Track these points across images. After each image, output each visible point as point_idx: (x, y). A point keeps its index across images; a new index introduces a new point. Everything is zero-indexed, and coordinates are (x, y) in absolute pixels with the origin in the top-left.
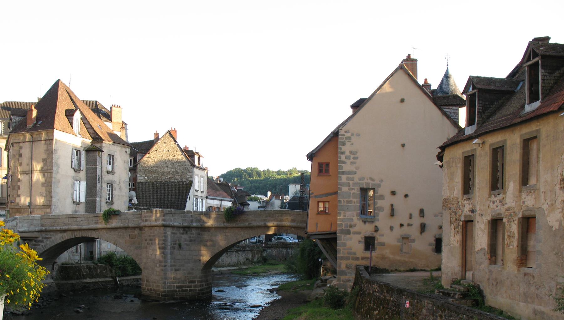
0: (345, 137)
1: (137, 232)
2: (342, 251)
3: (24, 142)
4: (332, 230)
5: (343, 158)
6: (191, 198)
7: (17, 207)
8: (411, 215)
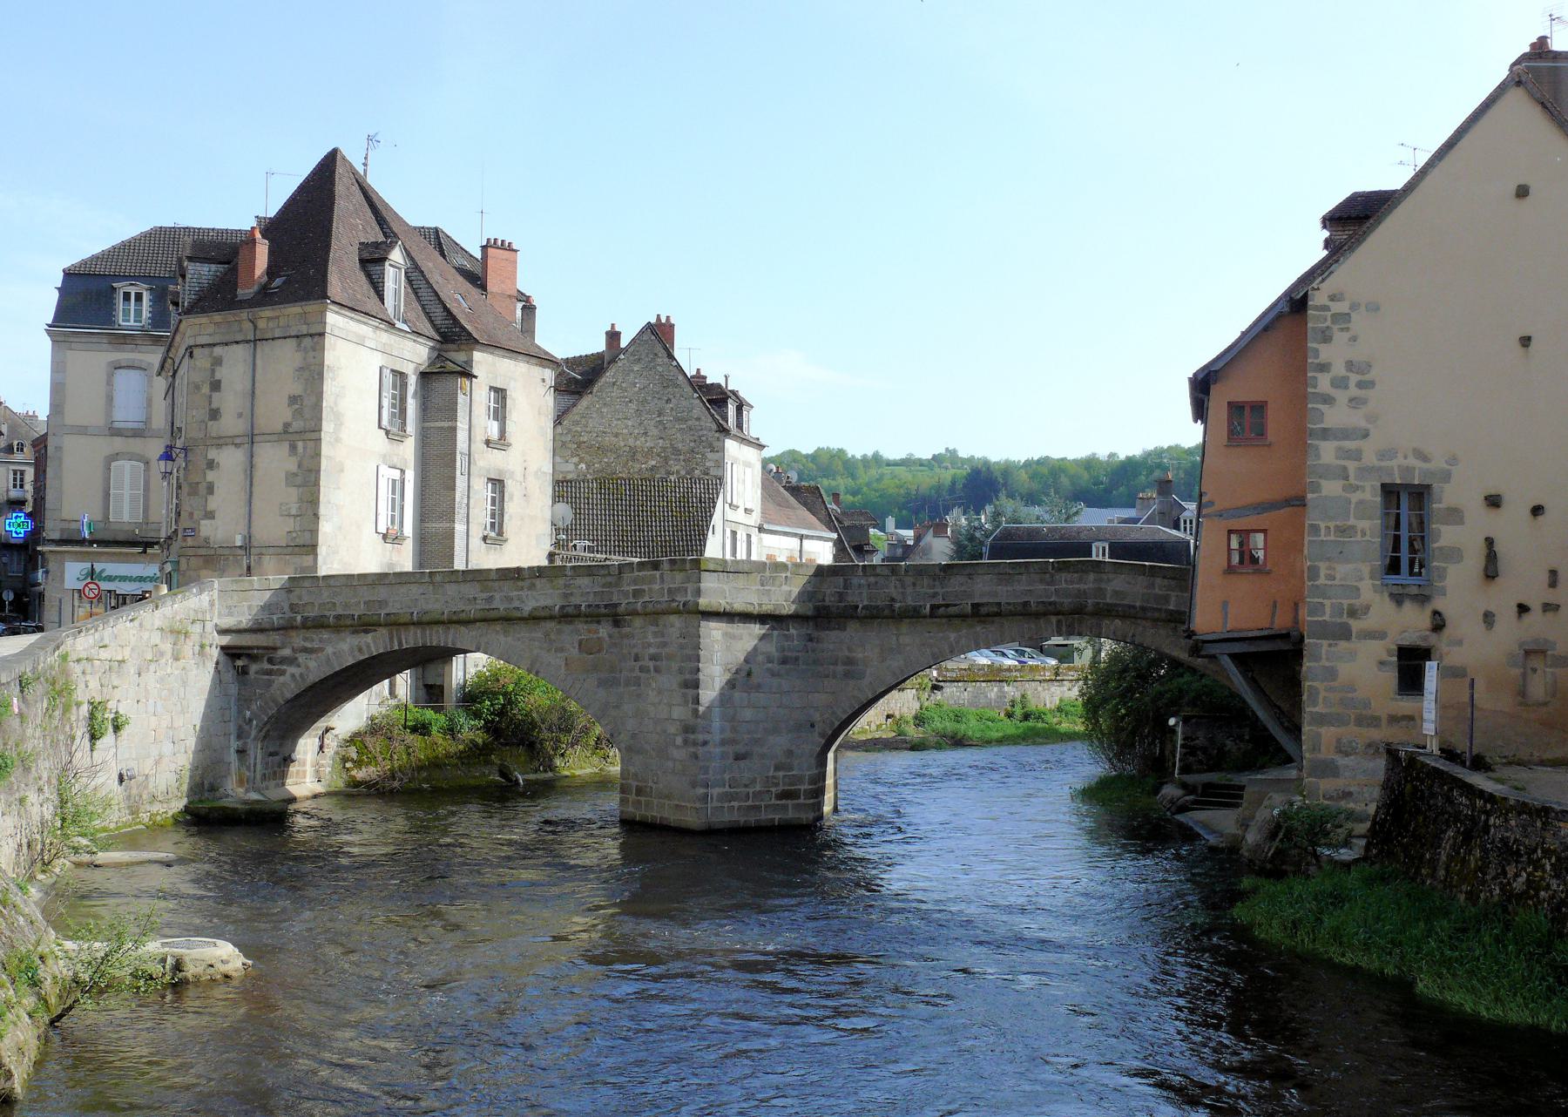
0: (1329, 314)
1: (604, 630)
2: (1321, 697)
3: (226, 344)
4: (1276, 626)
5: (1323, 383)
6: (719, 529)
7: (203, 552)
8: (1553, 573)
